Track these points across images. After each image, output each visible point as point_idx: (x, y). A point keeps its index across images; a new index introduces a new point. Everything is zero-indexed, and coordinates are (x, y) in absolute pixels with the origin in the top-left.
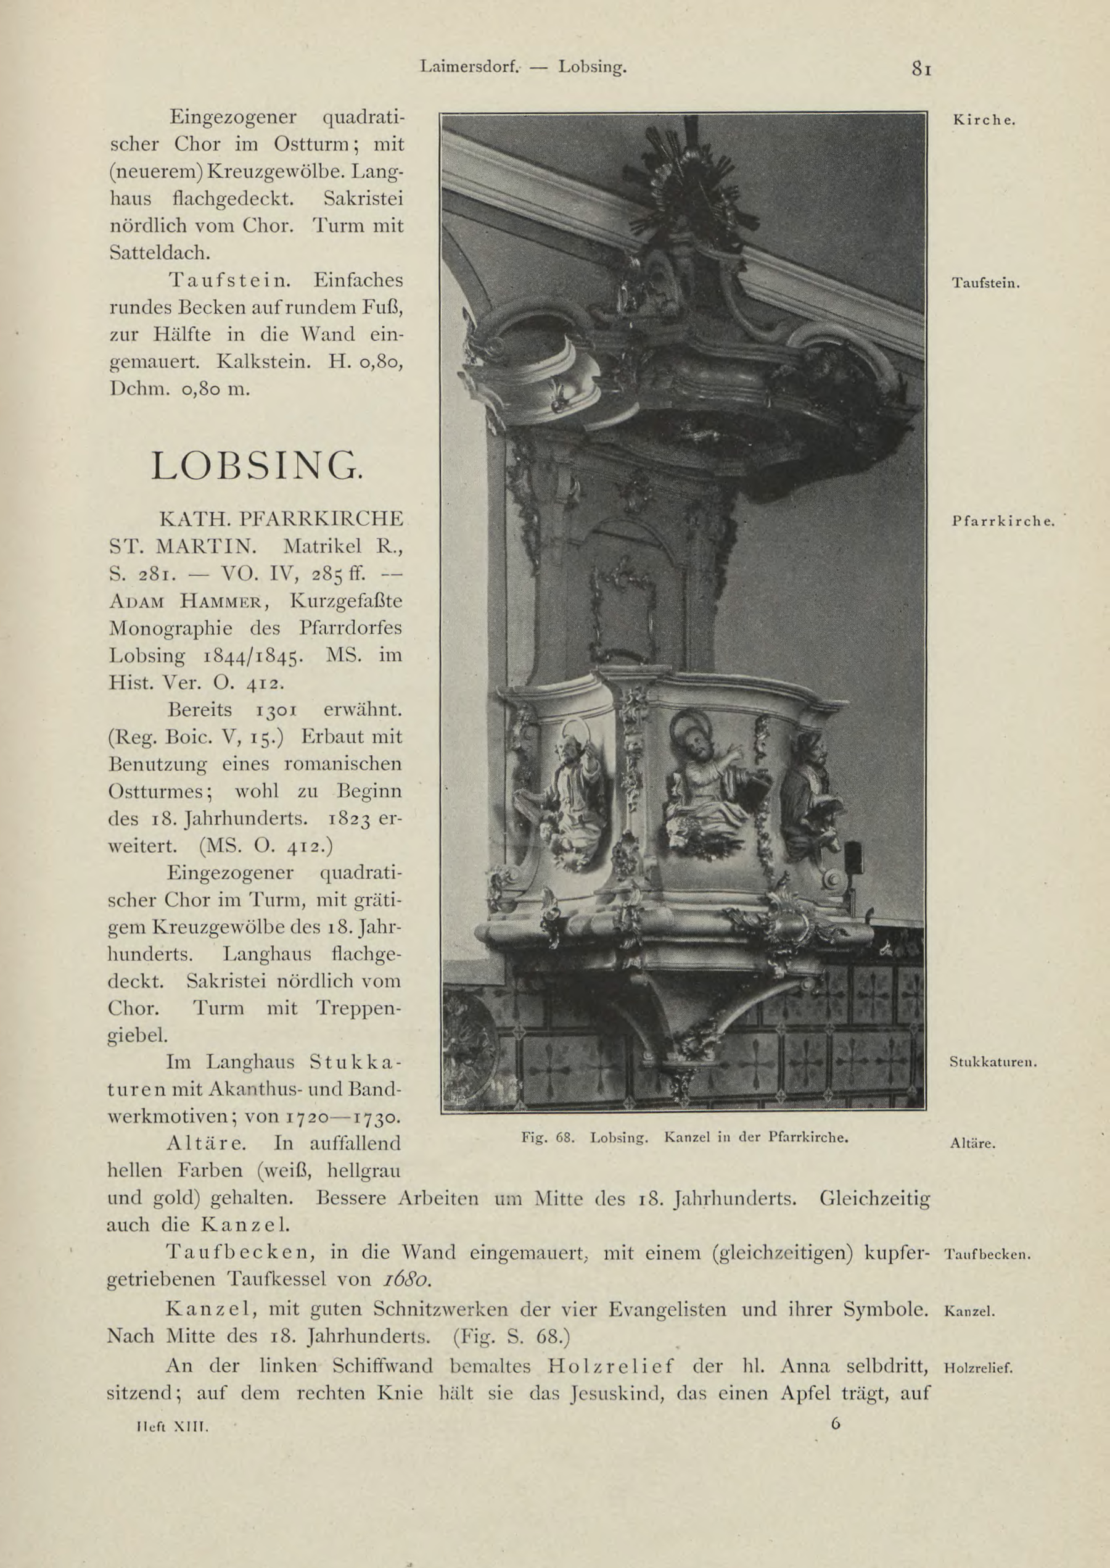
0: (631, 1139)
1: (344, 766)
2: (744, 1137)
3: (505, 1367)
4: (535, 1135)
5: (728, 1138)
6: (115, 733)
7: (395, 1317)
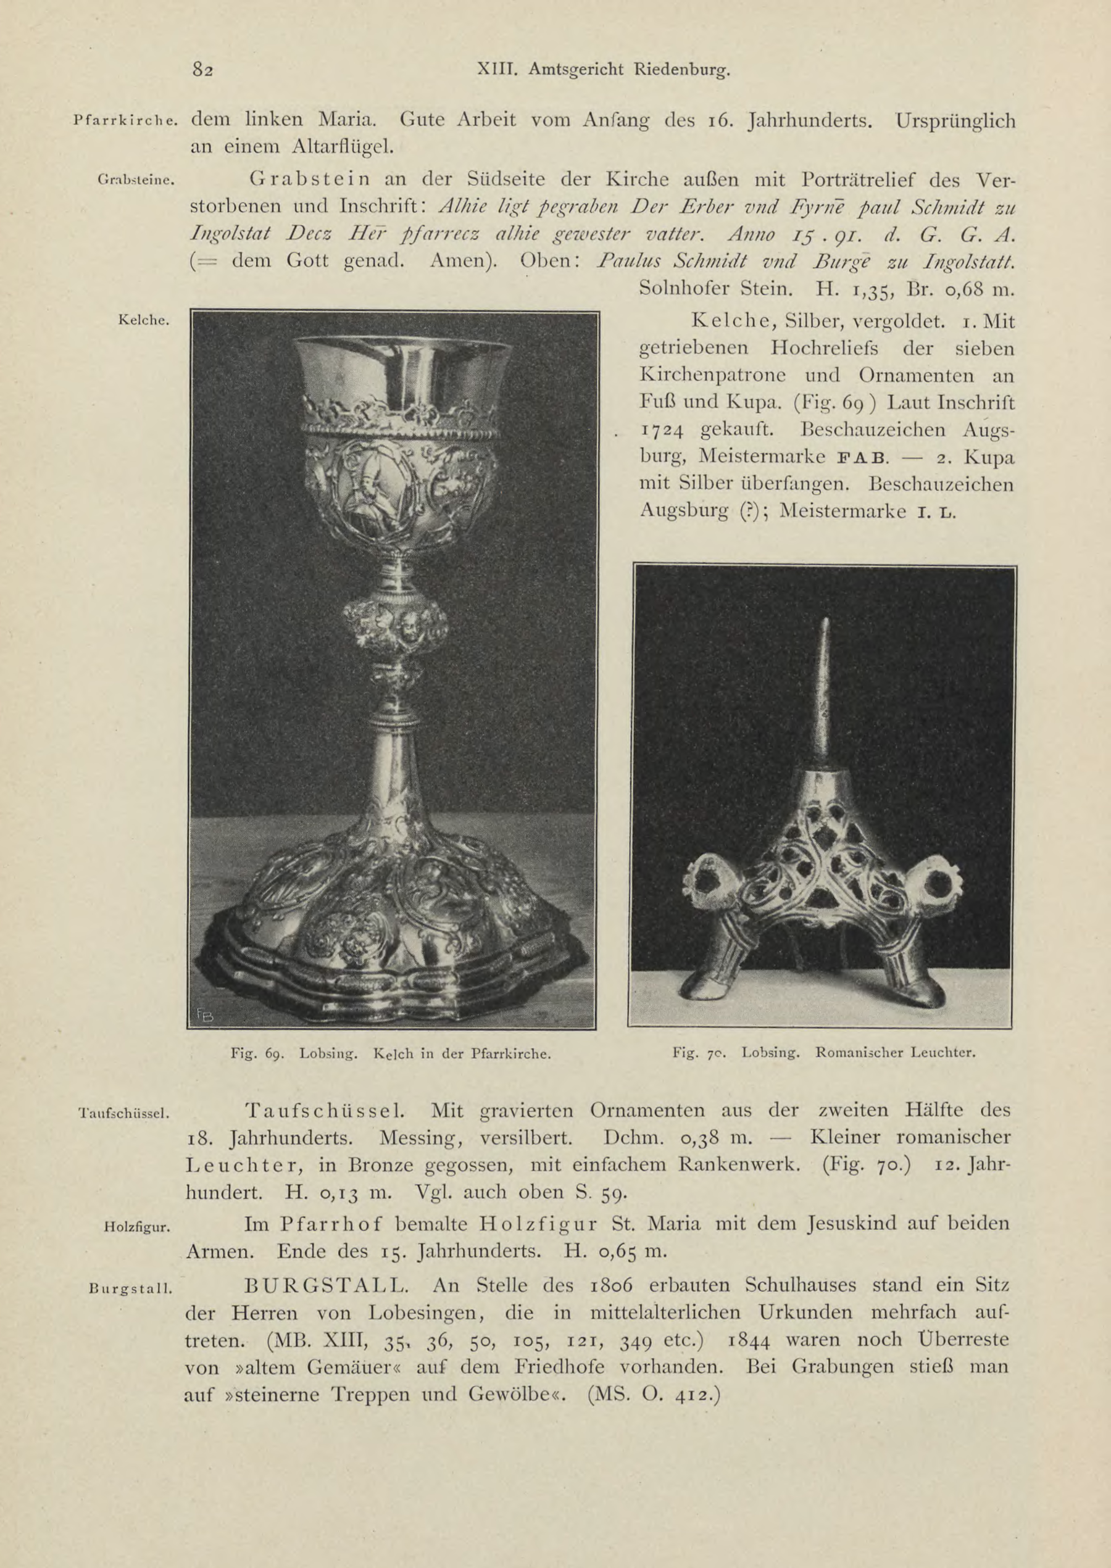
0: (341, 1055)
1: (956, 1140)
2: (447, 1054)
3: (451, 1224)
4: (244, 1051)
5: (431, 1055)
6: (830, 1160)
7: (843, 437)
